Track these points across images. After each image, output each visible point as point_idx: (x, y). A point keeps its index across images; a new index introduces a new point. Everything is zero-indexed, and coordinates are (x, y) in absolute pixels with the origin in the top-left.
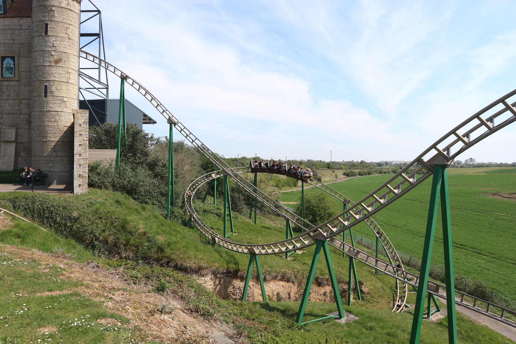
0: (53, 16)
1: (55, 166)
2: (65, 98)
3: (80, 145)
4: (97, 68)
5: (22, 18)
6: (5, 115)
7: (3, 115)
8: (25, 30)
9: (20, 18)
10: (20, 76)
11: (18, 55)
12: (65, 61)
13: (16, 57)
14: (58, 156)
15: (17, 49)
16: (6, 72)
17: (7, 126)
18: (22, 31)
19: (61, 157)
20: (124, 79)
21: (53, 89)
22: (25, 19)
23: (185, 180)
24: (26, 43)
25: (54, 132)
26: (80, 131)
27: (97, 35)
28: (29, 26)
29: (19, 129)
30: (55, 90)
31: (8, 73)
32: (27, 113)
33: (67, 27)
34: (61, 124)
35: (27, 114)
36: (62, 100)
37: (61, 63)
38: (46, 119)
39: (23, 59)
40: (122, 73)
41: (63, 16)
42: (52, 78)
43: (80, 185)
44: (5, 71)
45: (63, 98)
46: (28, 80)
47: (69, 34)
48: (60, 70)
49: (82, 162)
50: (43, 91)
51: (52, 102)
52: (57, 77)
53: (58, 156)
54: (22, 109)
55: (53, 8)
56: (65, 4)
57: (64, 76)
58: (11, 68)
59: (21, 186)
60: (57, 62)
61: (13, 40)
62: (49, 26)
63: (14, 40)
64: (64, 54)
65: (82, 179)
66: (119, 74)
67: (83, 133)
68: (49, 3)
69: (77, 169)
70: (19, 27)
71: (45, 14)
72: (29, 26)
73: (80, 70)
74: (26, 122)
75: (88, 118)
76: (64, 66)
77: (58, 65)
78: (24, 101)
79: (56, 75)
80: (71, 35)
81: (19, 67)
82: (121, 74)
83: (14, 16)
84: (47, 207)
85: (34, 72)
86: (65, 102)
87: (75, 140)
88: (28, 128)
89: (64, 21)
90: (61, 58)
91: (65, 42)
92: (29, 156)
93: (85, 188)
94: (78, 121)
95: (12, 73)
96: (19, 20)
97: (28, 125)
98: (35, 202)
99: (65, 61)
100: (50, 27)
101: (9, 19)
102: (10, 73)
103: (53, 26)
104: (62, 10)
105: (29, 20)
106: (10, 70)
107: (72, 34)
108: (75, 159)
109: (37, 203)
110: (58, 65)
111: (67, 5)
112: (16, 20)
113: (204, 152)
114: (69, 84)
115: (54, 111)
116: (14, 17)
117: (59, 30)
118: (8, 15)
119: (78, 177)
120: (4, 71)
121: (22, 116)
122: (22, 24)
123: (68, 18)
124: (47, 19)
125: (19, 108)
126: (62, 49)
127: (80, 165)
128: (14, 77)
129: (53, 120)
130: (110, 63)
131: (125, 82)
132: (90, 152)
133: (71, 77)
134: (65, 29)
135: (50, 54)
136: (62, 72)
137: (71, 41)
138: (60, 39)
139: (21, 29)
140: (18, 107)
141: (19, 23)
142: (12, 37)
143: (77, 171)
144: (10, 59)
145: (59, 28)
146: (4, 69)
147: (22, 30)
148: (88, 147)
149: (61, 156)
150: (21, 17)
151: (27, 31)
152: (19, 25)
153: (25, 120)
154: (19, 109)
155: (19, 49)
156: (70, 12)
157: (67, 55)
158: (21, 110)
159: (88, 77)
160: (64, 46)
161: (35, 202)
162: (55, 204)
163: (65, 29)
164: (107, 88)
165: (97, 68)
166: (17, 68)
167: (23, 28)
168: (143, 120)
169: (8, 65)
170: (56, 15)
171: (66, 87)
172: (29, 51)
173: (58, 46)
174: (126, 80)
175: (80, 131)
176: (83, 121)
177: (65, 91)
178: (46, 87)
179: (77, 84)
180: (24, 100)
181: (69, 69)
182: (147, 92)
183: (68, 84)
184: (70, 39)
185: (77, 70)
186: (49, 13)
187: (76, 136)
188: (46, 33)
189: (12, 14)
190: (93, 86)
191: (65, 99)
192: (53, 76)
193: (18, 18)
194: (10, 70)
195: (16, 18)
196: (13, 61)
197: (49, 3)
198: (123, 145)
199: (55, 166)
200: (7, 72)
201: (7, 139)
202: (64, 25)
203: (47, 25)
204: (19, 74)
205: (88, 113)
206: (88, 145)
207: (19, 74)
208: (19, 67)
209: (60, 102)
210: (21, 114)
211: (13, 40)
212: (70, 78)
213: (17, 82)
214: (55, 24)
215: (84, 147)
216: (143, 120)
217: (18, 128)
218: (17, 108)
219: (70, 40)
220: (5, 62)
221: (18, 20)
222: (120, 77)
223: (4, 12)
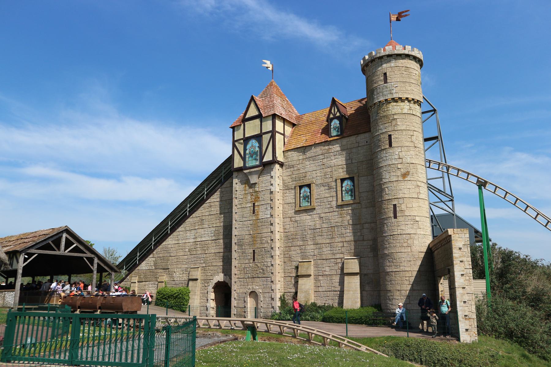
0: (396, 125)
1: (412, 302)
2: (417, 217)
3: (462, 275)
4: (441, 177)
5: (359, 135)
8: (363, 147)
10: (361, 197)
11: (357, 174)
12: (413, 174)
13: (355, 178)
14: (414, 290)
15: (356, 168)
16: (346, 195)
18: (359, 148)
19: (418, 291)
20: (482, 185)
21: (403, 207)
22: (362, 135)
24: (364, 160)
25: (409, 259)
26: (460, 257)
27: (436, 138)
28: (367, 142)
29: (363, 258)
30: (406, 209)
32: (370, 239)
33: (412, 134)
34: (415, 249)
35: (371, 240)
36: (414, 220)
37: (409, 176)
38: (398, 245)
39: (363, 178)
40: (478, 178)
41: (406, 123)
42: (401, 195)
43: (467, 330)
45: (414, 217)
46: (369, 201)
47: (414, 141)
48: (409, 185)
49: (466, 298)
50: (392, 212)
51: (403, 223)
52: (406, 193)
53: (414, 290)
54: (365, 234)
55: (395, 117)
56: (407, 110)
57: (413, 191)
60: (405, 175)
61: (351, 160)
62: (392, 136)
63: (352, 159)
64: (411, 165)
65: (469, 321)
66: (475, 180)
67: (464, 259)
68: (390, 112)
69: (461, 308)
70: (356, 145)
71: (387, 125)
73: (429, 182)
74: (369, 249)
75: (468, 239)
76: (412, 179)
77: (406, 179)
78: (366, 226)
79: (405, 191)
80: (416, 143)
81: (359, 188)
82: (478, 180)
83: (352, 134)
84: (439, 360)
85: (378, 191)
86: (417, 222)
87: (455, 269)
88: (372, 256)
89: (408, 129)
90: (409, 171)
91: (411, 152)
92: (376, 291)
93: (474, 335)
94: (457, 244)
95: (308, 202)
97: (372, 253)
98: (420, 351)
99: (413, 174)
100: (394, 137)
101: (346, 138)
103: (397, 136)
104: (404, 117)
105: (367, 135)
107: (417, 141)
108: (457, 294)
109: (425, 354)
110: (406, 179)
111: (409, 110)
112: (353, 139)
114: (420, 200)
115: (405, 234)
116: (351, 136)
117: (404, 139)
118: (345, 135)
119: (463, 318)
120: (343, 195)
121: (365, 243)
122: (360, 141)
123: (411, 124)
124: (390, 130)
125: (361, 234)
126: (409, 160)
127: (465, 302)
128: (311, 205)
129: (405, 245)
132: (475, 284)
133: (421, 192)
134: (410, 136)
135: (397, 168)
136: (411, 187)
137: (417, 149)
138: (406, 148)
140: (360, 233)
141: (356, 141)
142: (350, 157)
143: (461, 310)
145: (403, 136)
146: (247, 156)
147: (360, 148)
148: (472, 278)
149: (419, 290)
150: (358, 134)
151: (365, 147)
152: (356, 143)
153: (369, 247)
154: (361, 235)
155: (358, 168)
156: (412, 117)
157: (414, 166)
158: (363, 235)
159: (437, 190)
160: (410, 156)
161: (420, 351)
162: (447, 356)
163: (410, 136)
164: (452, 200)
165: (441, 177)
166: (356, 190)
167: (360, 145)
170: (399, 123)
171: (417, 204)
172: (368, 168)
173: (404, 157)
174: (485, 186)
175: (460, 257)
176: (463, 243)
177: (416, 209)
178: (395, 206)
179: (427, 199)
180: (366, 224)
181: (418, 182)
183: (419, 199)
184: (415, 147)
185: (426, 182)
186: (391, 123)
188: (390, 145)
189: (349, 133)
190: (440, 199)
191: (417, 219)
192: (402, 192)
193: (355, 136)
195: (353, 136)
196: (309, 189)
197: (390, 112)
198: (491, 273)
199: (412, 302)
202: (408, 133)
203: (390, 136)
204: (359, 195)
205: (468, 232)
206: (472, 275)
207: (359, 195)
208: (359, 188)
209: (412, 223)
210: (363, 240)
211: (351, 160)
212: (420, 193)
213: (358, 205)
214: (399, 134)
215: (467, 278)
216: (476, 237)
217: (361, 257)
218: (359, 234)
219: (415, 148)
220: (302, 191)
221: (355, 138)
223: (341, 132)
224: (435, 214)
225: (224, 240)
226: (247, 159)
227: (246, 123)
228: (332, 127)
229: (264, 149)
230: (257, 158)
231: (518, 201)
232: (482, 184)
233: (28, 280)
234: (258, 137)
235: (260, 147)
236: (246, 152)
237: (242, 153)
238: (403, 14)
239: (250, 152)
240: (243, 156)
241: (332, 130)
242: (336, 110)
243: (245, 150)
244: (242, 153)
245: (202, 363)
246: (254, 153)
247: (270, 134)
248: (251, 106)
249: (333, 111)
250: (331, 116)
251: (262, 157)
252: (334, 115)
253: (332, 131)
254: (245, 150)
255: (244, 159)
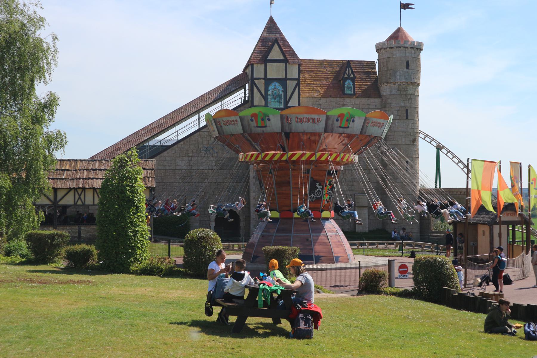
6: (356, 183)
7: (354, 183)
9: (368, 99)
17: (357, 193)
23: (522, 351)
28: (376, 106)
31: (275, 102)
44: (271, 99)
58: (280, 96)
59: (258, 297)
72: (376, 106)
96: (367, 100)
102: (277, 102)
106: (278, 98)
113: (319, 78)
130: (506, 241)
131: (440, 151)
139: (369, 108)
144: (277, 84)
146: (269, 97)
152: (367, 104)
167: (370, 107)
168: (318, 118)
169: (275, 92)
174: (441, 149)
182: (455, 156)
187: (265, 319)
188: (407, 118)
194: (278, 98)
200: (273, 100)
201: (361, 204)
203: (407, 111)
222: (436, 147)
224: (523, 187)
225: (465, 191)
226: (269, 100)
227: (268, 64)
228: (346, 86)
229: (289, 94)
230: (281, 100)
231: (264, 104)
232: (439, 148)
233: (271, 201)
234: (283, 81)
235: (285, 91)
236: (267, 93)
237: (263, 92)
238: (410, 6)
239: (272, 93)
240: (264, 95)
241: (346, 88)
242: (350, 72)
243: (266, 90)
244: (263, 92)
245: (225, 273)
246: (277, 95)
247: (296, 82)
248: (273, 48)
249: (347, 72)
250: (346, 76)
251: (287, 102)
252: (349, 76)
253: (346, 90)
254: (266, 90)
255: (265, 98)
